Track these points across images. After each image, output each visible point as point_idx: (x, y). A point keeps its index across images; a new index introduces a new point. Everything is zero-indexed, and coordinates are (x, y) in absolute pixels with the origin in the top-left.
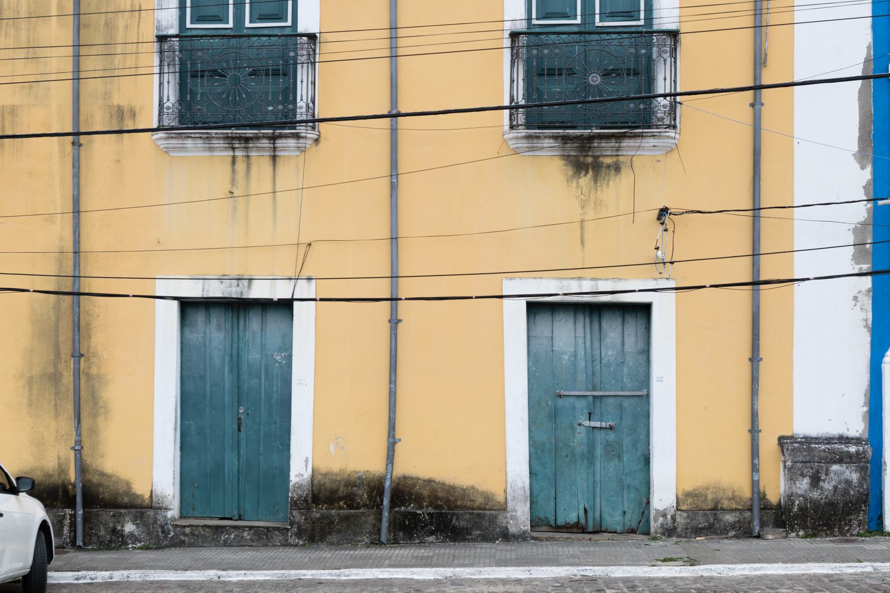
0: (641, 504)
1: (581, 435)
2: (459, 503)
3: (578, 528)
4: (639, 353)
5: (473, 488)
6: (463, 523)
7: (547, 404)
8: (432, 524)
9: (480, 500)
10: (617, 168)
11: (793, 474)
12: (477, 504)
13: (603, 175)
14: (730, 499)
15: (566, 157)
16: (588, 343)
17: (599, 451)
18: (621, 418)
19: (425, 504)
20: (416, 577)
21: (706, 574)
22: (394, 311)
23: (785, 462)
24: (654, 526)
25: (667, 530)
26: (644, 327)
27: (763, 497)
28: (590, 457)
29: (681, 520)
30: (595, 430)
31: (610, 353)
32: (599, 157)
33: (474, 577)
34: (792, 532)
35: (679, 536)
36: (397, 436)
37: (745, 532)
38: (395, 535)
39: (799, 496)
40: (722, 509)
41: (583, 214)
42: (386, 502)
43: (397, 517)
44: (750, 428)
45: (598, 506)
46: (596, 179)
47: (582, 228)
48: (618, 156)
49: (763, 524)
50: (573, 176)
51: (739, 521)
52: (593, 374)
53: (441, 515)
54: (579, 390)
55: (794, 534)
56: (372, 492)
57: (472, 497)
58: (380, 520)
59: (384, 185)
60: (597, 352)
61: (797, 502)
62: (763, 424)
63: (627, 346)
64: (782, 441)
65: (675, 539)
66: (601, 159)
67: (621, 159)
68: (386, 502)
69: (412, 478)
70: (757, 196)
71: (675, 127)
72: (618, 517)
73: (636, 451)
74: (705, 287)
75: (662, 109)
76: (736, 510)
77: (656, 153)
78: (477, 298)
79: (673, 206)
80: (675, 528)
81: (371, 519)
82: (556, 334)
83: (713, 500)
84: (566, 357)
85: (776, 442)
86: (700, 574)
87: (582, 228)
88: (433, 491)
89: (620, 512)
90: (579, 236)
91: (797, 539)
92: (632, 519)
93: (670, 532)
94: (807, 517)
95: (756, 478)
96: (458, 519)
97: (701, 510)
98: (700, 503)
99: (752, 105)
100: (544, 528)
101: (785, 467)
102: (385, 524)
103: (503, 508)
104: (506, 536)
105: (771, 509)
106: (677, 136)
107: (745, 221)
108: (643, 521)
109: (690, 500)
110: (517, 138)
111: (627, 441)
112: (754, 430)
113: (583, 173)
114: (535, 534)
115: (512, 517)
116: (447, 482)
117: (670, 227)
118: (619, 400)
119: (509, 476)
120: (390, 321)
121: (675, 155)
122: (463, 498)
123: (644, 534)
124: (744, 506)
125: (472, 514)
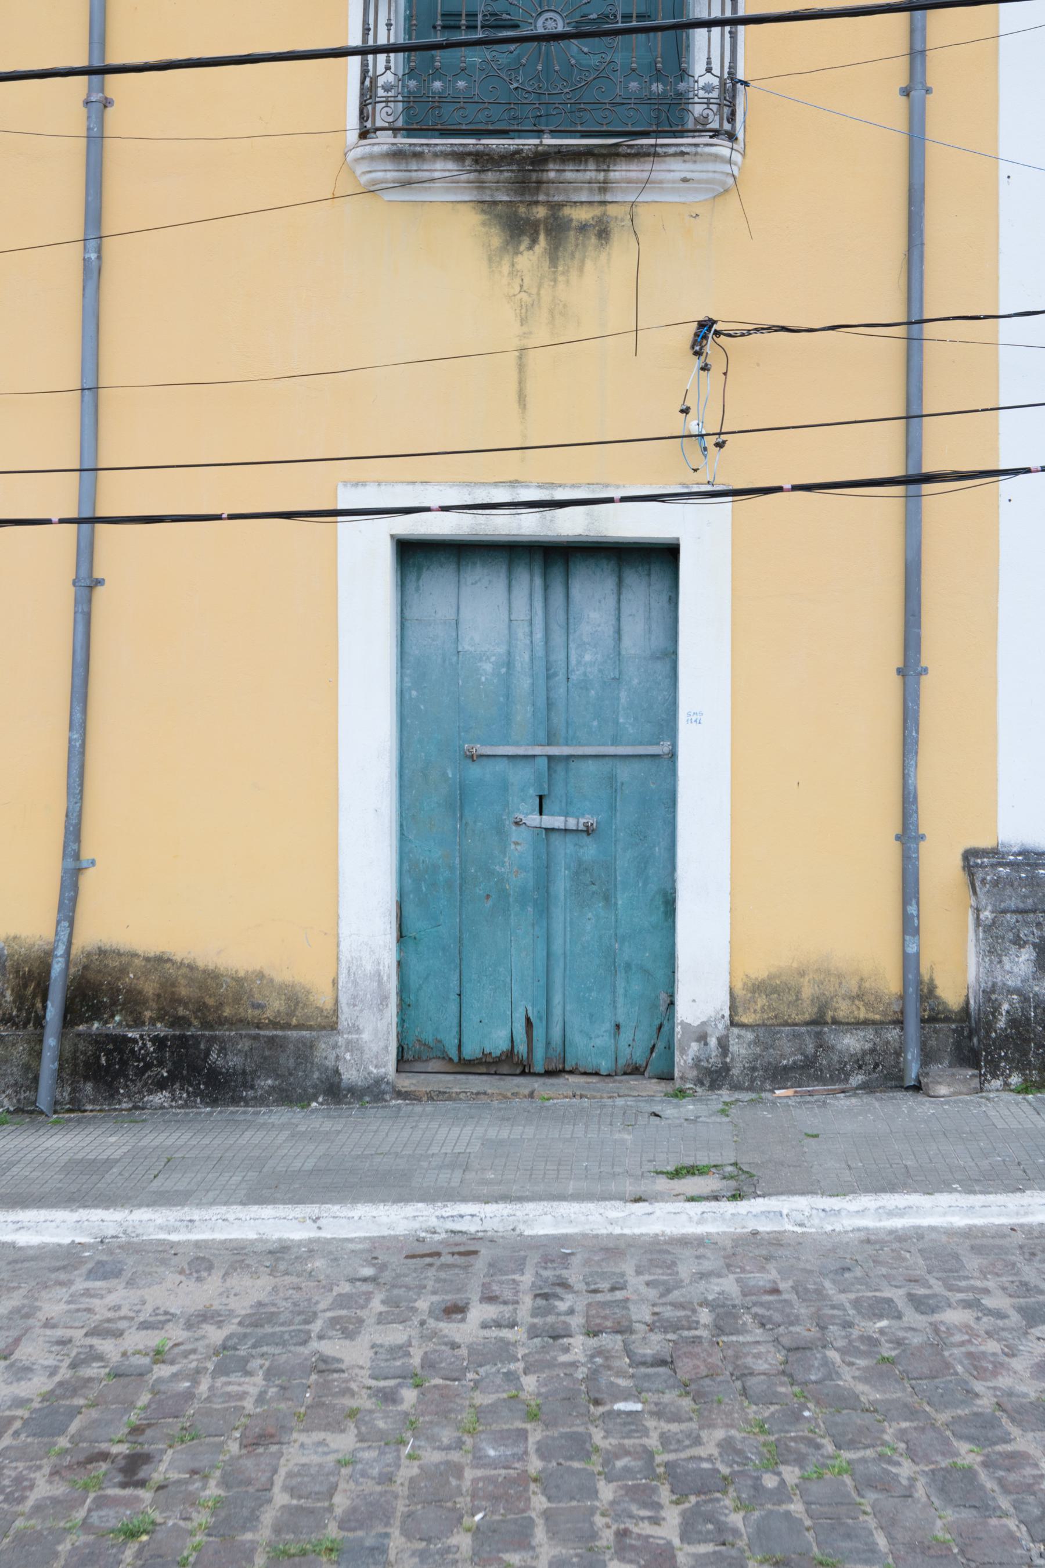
0: (655, 1006)
1: (520, 846)
2: (227, 1012)
3: (511, 1064)
4: (655, 657)
5: (261, 975)
6: (234, 1061)
7: (444, 774)
8: (161, 1063)
9: (276, 1005)
10: (603, 233)
11: (995, 939)
12: (269, 1014)
13: (570, 248)
14: (852, 999)
15: (487, 206)
16: (539, 635)
17: (561, 885)
18: (613, 808)
19: (148, 1014)
20: (23, 1239)
21: (765, 1227)
22: (86, 553)
23: (978, 911)
24: (683, 1061)
25: (708, 1072)
26: (665, 598)
27: (927, 993)
28: (542, 899)
29: (740, 1048)
30: (554, 837)
31: (588, 657)
32: (561, 205)
33: (174, 1237)
34: (995, 1076)
35: (736, 1087)
36: (86, 854)
37: (887, 1076)
38: (74, 1090)
39: (1010, 991)
40: (835, 1022)
41: (525, 335)
42: (53, 1012)
43: (81, 1046)
44: (899, 830)
45: (557, 1011)
46: (553, 256)
47: (521, 367)
48: (603, 203)
49: (928, 1057)
50: (504, 249)
51: (873, 1051)
52: (550, 705)
53: (183, 1040)
54: (517, 744)
55: (997, 1083)
56: (26, 986)
57: (258, 999)
58: (39, 1055)
59: (70, 261)
60: (559, 656)
61: (1005, 1007)
62: (928, 821)
63: (626, 642)
64: (971, 859)
65: (725, 1094)
66: (567, 211)
67: (612, 210)
68: (53, 1012)
69: (119, 954)
70: (915, 295)
71: (732, 137)
72: (602, 1038)
73: (645, 884)
74: (779, 489)
75: (701, 93)
76: (866, 1023)
77: (690, 198)
78: (232, 517)
79: (725, 317)
80: (727, 1068)
81: (19, 1052)
82: (466, 614)
83: (815, 999)
84: (488, 667)
85: (958, 862)
86: (752, 1225)
87: (521, 367)
88: (168, 985)
89: (608, 1026)
90: (513, 387)
91: (1006, 1096)
92: (633, 1044)
93: (715, 1077)
94: (1028, 1041)
95: (912, 949)
96: (223, 1050)
97: (786, 1024)
98: (783, 1008)
99: (906, 92)
100: (433, 1065)
101: (978, 921)
102: (49, 1065)
103: (330, 1025)
104: (335, 1091)
105: (947, 1020)
106: (737, 157)
107: (890, 348)
108: (660, 1046)
109: (762, 1001)
110: (372, 157)
111: (625, 861)
112: (909, 837)
113: (526, 241)
114: (406, 1083)
115: (350, 1046)
116: (201, 964)
117: (717, 364)
118: (605, 766)
119: (344, 947)
120: (74, 583)
121: (732, 199)
122: (237, 1000)
123: (661, 1078)
124: (884, 1013)
125: (256, 1038)
